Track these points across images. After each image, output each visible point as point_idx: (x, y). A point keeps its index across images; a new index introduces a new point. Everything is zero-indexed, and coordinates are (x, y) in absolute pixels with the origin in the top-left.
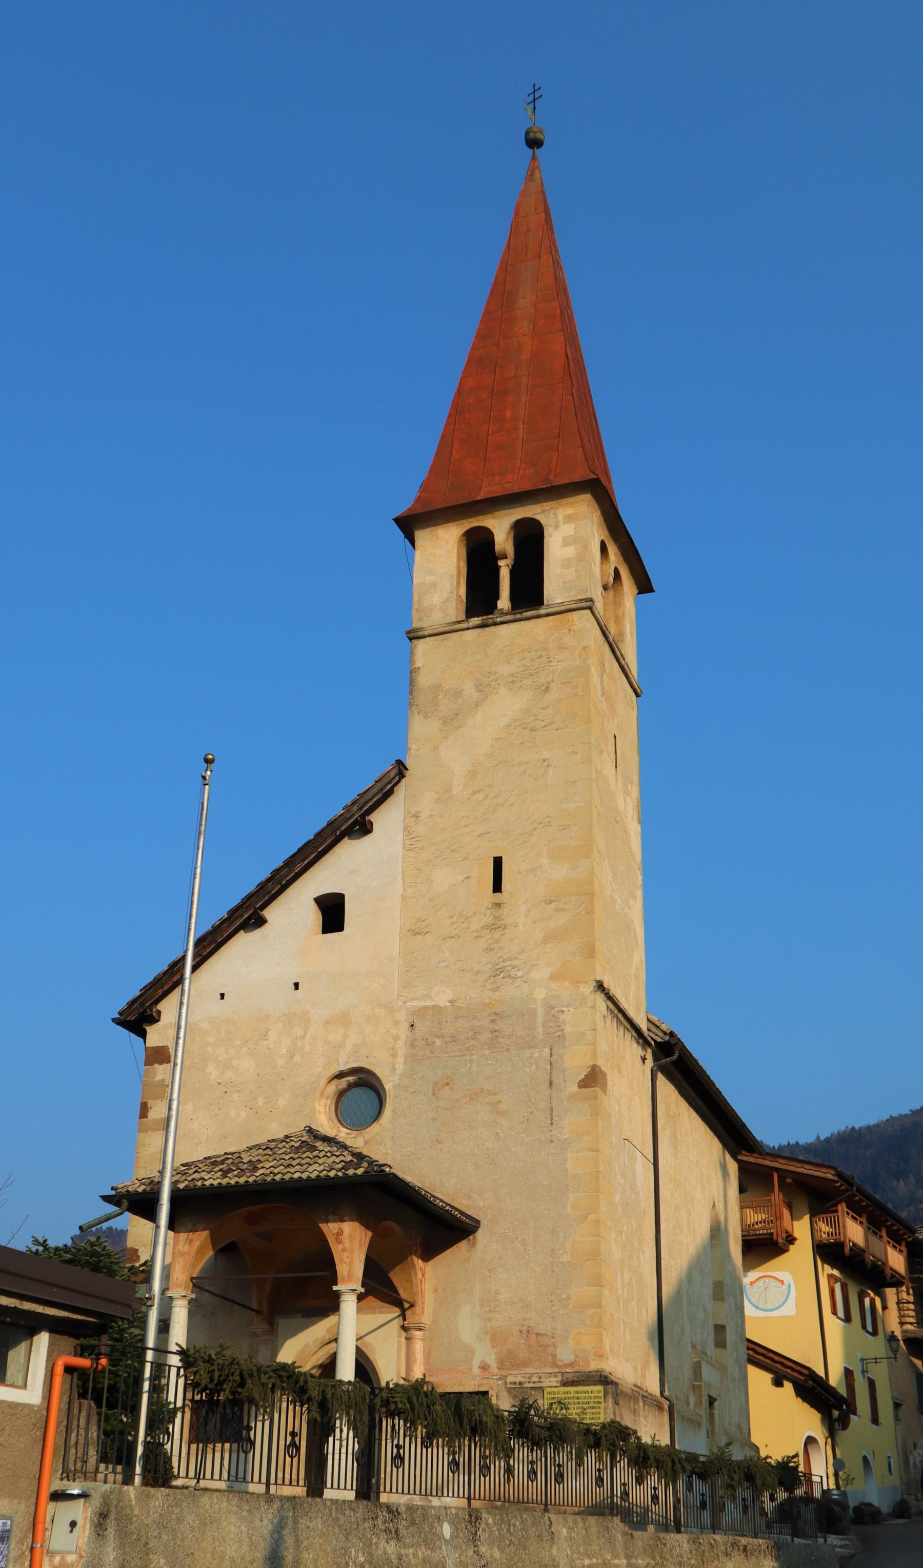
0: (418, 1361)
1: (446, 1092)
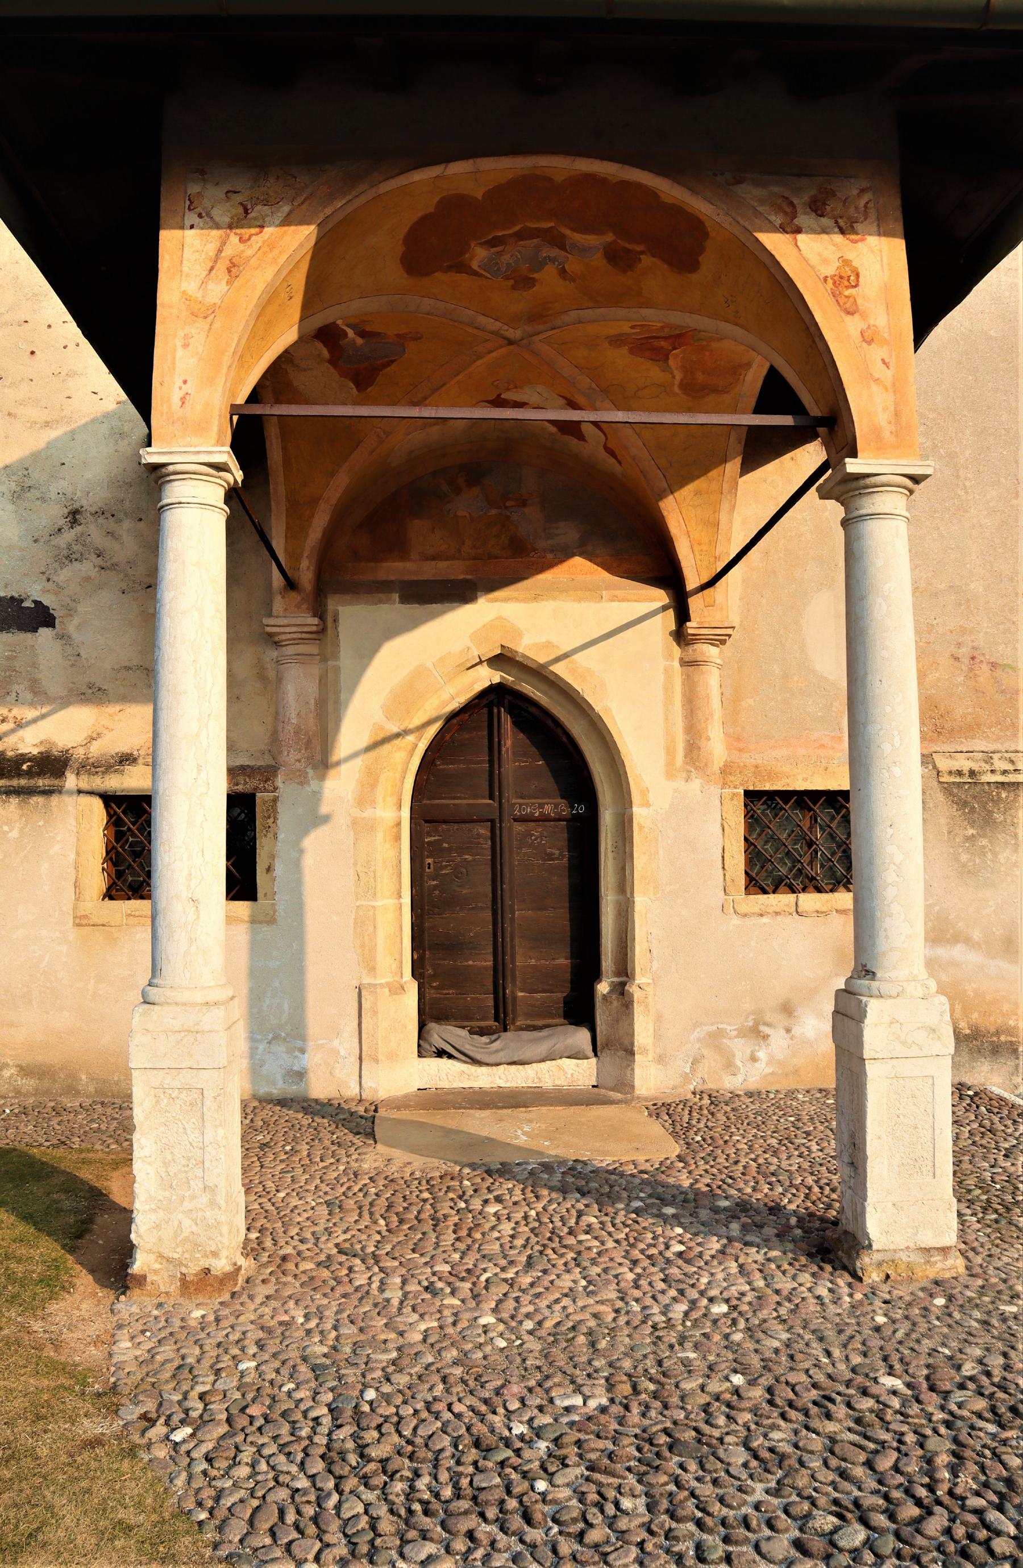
0: (716, 717)
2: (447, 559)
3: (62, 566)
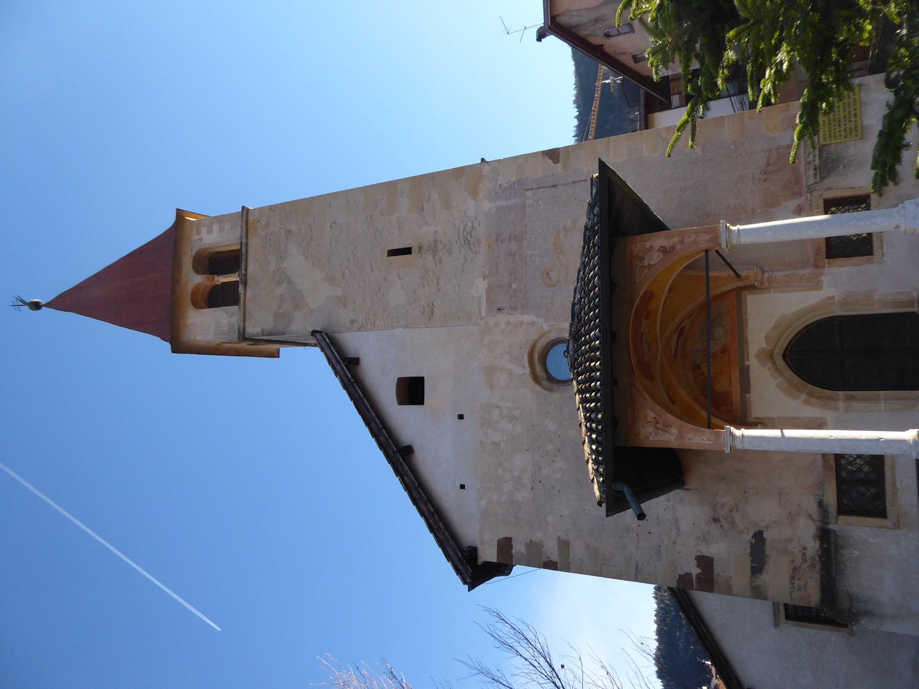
1: (553, 275)
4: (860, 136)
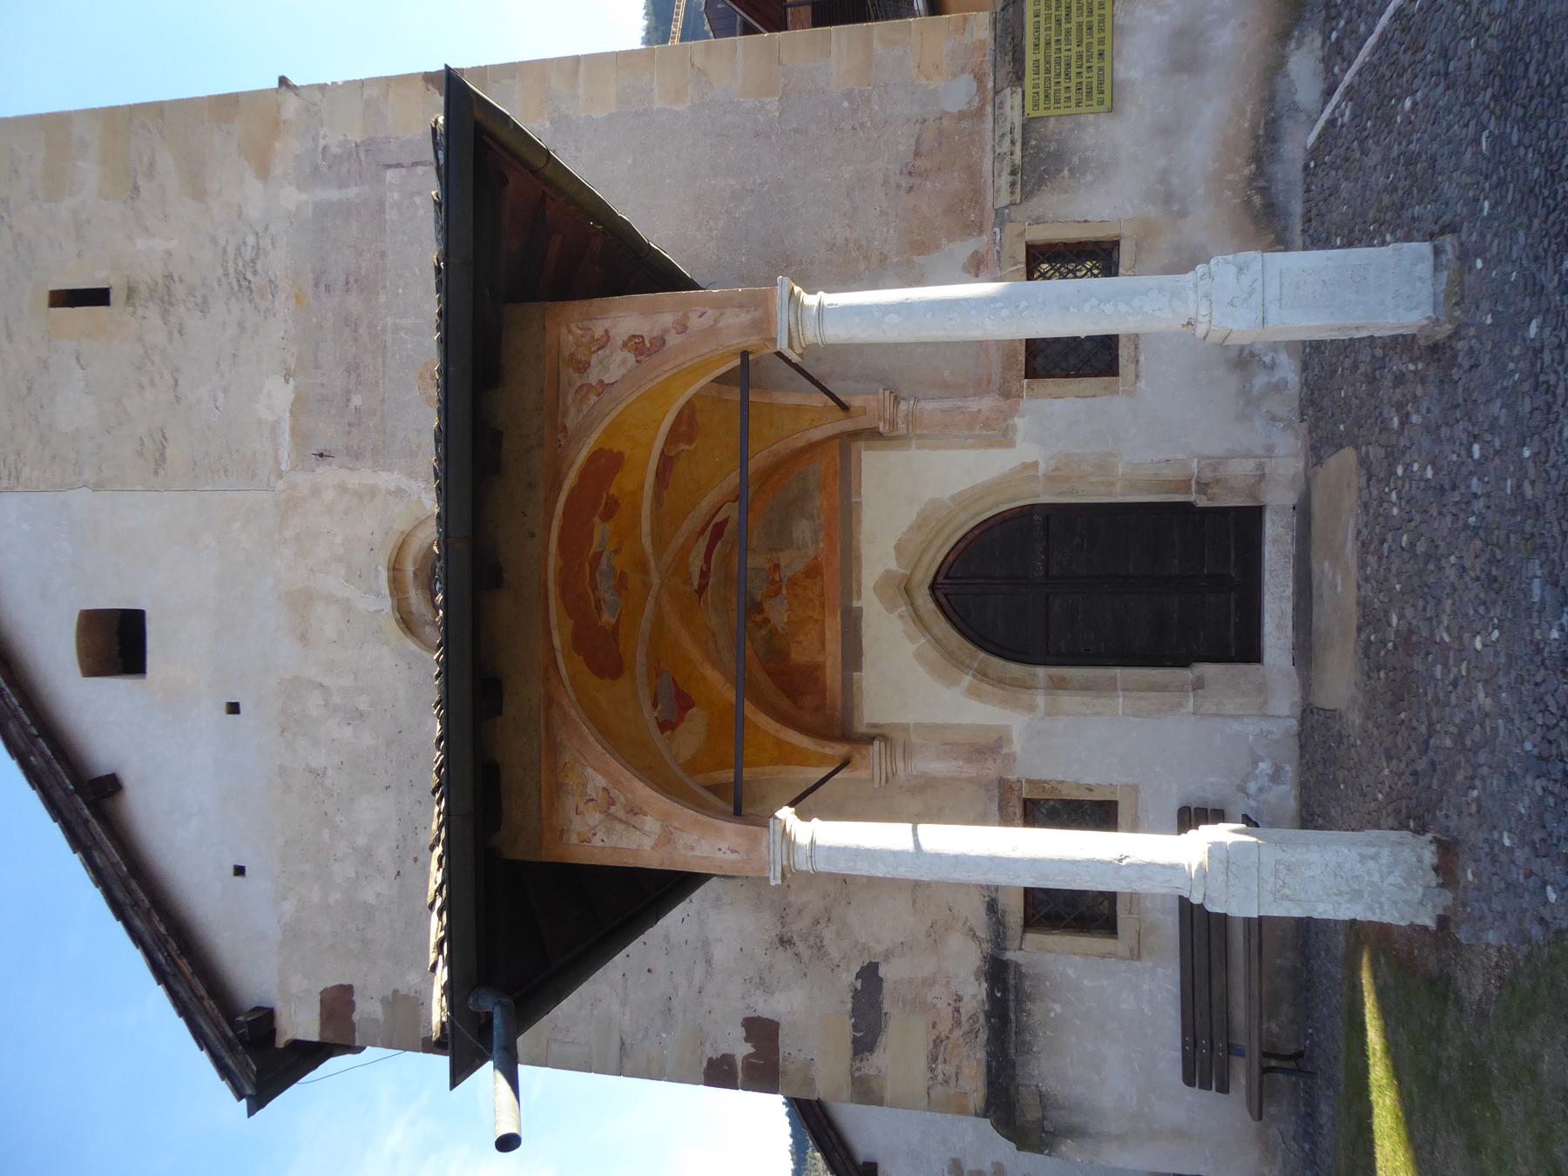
2: (823, 631)
3: (826, 954)
4: (1107, 102)
